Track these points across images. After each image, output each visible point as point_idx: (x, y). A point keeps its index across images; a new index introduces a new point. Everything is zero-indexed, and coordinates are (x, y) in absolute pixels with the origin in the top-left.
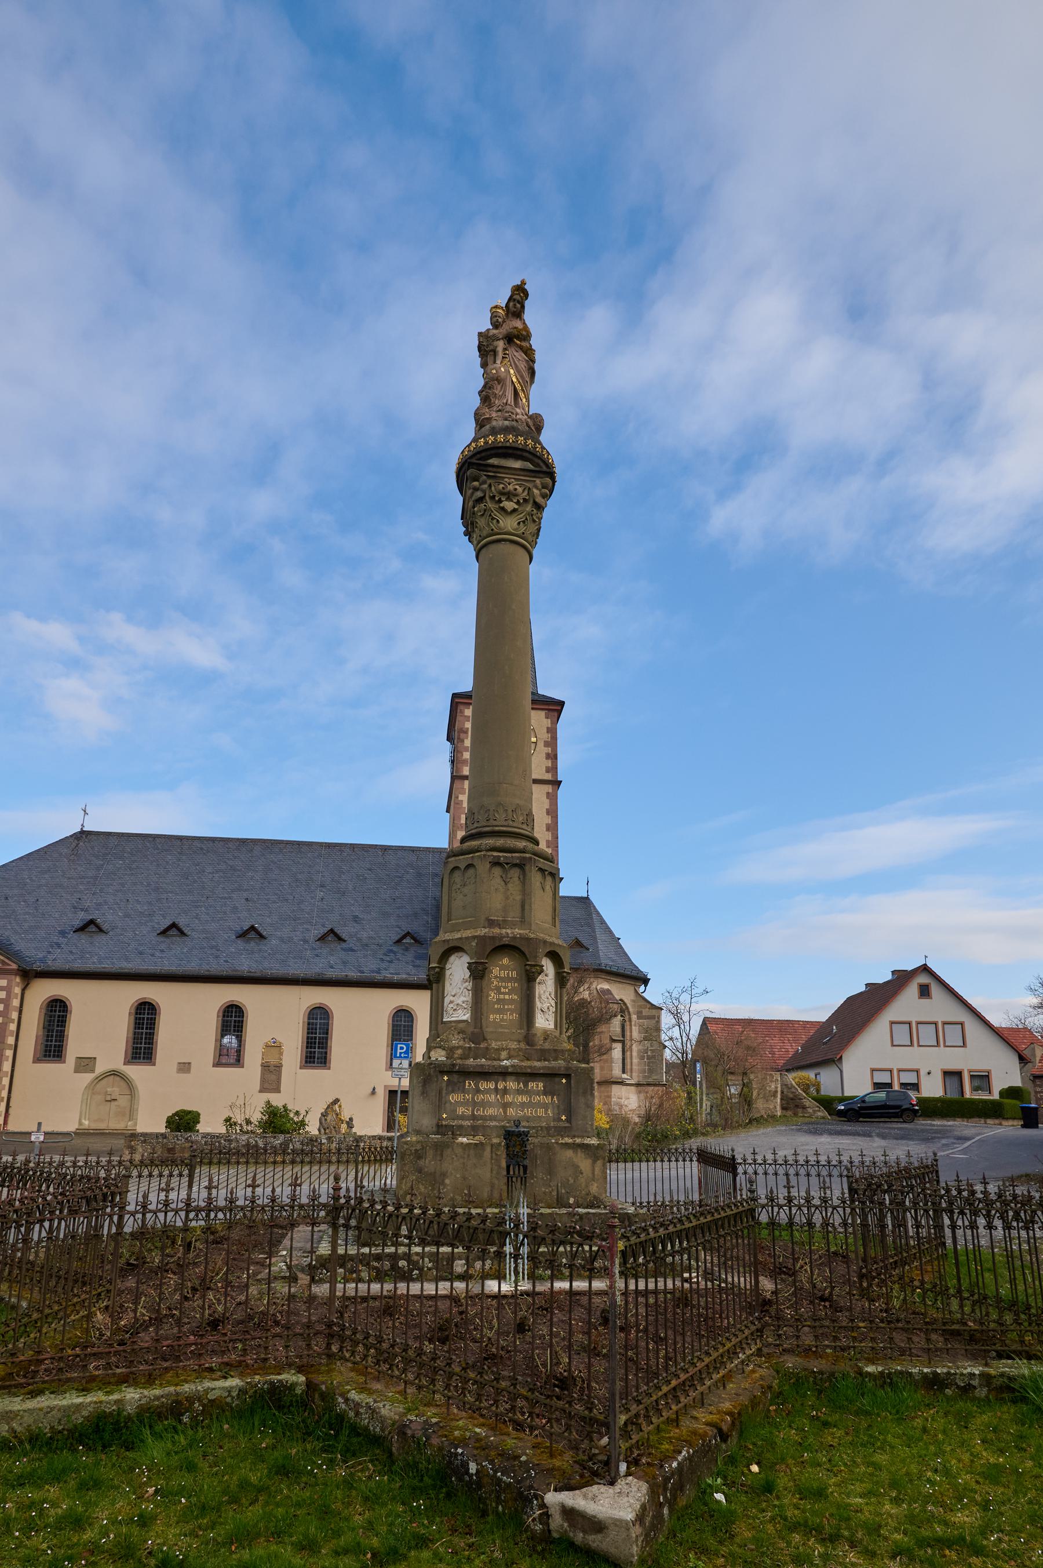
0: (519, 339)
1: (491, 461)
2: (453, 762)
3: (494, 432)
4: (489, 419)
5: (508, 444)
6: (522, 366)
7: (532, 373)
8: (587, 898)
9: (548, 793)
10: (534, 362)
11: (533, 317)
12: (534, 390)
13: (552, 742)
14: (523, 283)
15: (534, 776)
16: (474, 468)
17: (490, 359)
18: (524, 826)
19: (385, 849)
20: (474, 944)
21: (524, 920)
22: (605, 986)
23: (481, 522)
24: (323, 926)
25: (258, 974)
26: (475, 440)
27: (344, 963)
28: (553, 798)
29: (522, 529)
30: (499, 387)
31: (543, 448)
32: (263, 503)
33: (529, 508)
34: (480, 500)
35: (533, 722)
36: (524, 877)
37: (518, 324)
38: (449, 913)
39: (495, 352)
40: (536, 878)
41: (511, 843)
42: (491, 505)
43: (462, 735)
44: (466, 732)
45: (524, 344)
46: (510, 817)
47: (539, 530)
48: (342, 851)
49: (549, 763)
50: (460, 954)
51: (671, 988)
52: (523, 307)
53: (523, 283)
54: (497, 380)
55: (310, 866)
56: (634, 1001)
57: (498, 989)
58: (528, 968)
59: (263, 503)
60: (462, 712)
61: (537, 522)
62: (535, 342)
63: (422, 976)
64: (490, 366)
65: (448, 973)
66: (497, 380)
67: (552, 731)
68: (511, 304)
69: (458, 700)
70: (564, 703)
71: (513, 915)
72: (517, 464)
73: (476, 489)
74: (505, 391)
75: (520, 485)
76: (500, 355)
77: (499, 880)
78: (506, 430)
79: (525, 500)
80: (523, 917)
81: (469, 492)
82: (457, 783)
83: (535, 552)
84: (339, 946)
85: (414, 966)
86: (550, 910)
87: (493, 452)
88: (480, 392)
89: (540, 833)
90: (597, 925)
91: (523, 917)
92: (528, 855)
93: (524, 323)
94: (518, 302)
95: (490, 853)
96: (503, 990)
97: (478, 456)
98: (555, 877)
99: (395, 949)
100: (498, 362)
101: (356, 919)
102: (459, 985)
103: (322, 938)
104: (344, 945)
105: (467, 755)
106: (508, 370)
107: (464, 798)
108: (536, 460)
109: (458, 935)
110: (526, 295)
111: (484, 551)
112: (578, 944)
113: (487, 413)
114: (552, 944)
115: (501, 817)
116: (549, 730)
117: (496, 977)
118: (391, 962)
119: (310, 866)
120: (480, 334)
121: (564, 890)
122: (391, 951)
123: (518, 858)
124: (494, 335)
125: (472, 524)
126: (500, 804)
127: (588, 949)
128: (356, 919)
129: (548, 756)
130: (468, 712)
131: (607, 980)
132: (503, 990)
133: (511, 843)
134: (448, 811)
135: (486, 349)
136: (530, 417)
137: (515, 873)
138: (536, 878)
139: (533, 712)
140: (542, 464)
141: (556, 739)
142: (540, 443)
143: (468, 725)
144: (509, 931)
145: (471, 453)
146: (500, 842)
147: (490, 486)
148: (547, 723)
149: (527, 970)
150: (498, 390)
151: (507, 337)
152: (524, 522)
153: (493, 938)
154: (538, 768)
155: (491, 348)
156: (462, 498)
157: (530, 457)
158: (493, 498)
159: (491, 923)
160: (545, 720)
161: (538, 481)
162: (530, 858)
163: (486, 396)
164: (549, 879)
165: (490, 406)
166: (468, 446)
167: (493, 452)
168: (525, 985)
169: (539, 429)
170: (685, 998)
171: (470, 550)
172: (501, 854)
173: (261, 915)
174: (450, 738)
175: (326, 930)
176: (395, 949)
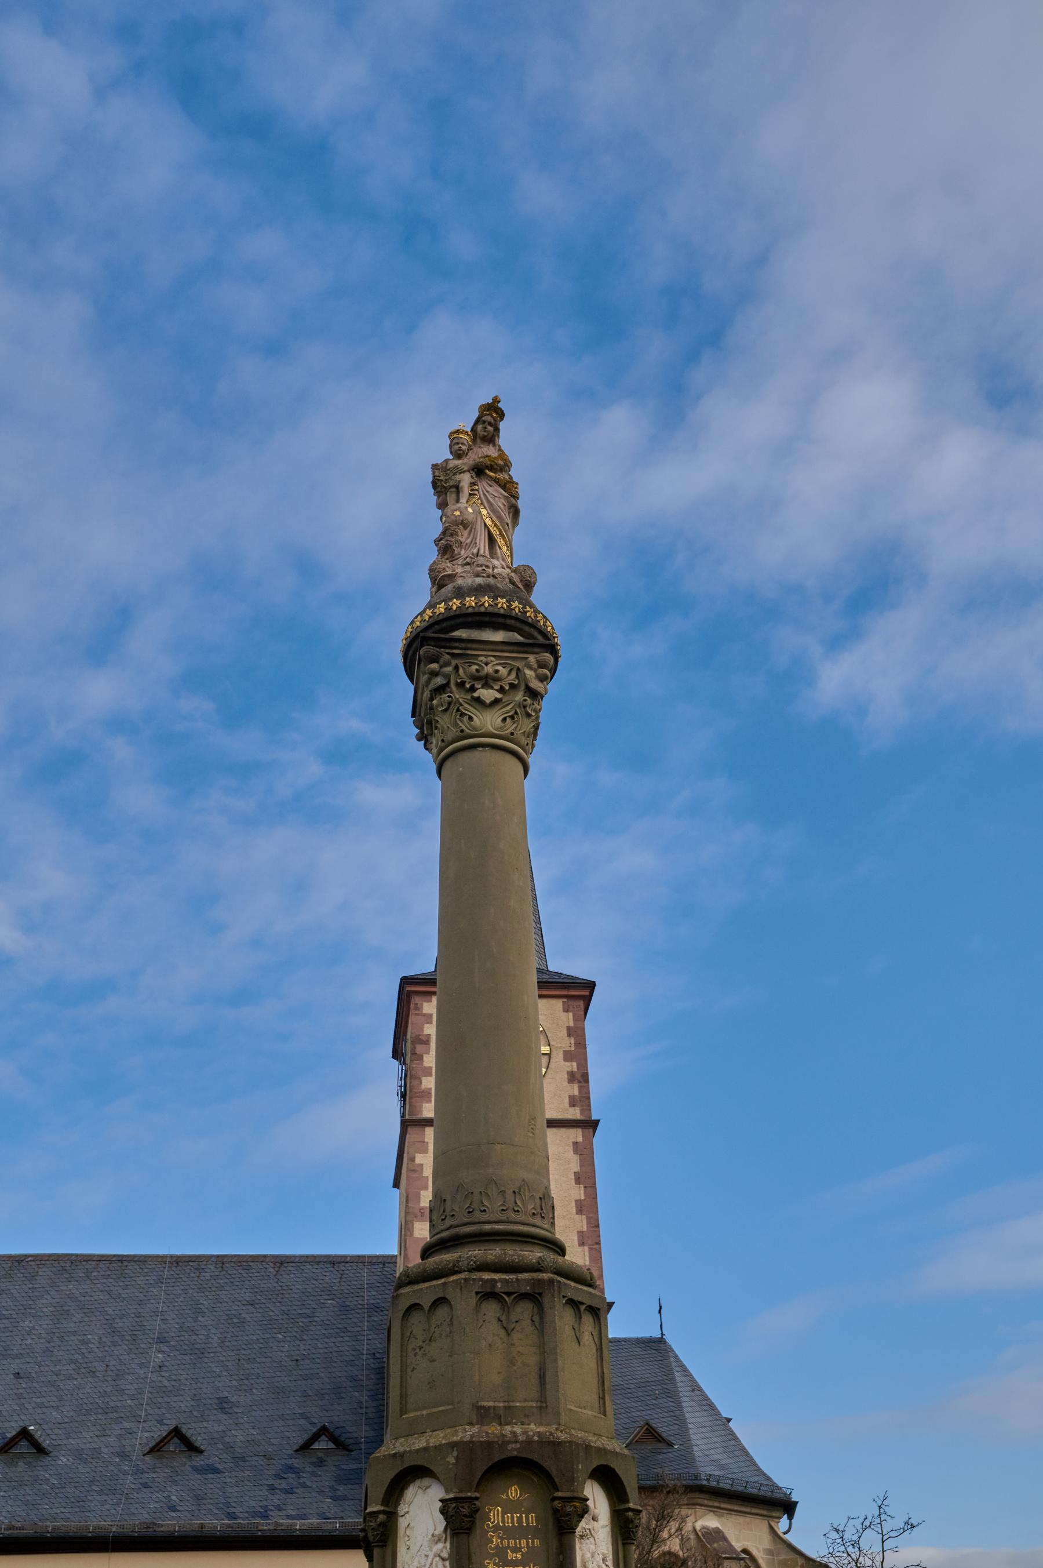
0: (492, 470)
1: (457, 634)
2: (403, 1095)
4: (452, 577)
5: (482, 609)
6: (500, 504)
7: (515, 512)
8: (661, 1341)
9: (576, 1144)
10: (516, 497)
11: (511, 437)
12: (518, 536)
13: (578, 1053)
14: (496, 400)
15: (551, 1114)
16: (430, 646)
17: (451, 498)
18: (537, 1221)
19: (281, 1262)
20: (451, 1460)
21: (545, 1404)
22: (710, 1522)
23: (444, 721)
24: (160, 1422)
25: (28, 1532)
26: (431, 605)
27: (198, 1498)
28: (584, 1152)
29: (510, 726)
31: (537, 612)
32: (100, 692)
33: (519, 696)
35: (542, 1019)
36: (541, 1318)
37: (492, 451)
38: (403, 1398)
39: (457, 489)
40: (563, 1319)
41: (513, 1253)
42: (458, 695)
43: (419, 1048)
44: (426, 1042)
45: (500, 476)
46: (511, 1205)
47: (536, 728)
48: (199, 1270)
49: (575, 1090)
50: (426, 1481)
51: (840, 1521)
52: (497, 430)
53: (496, 400)
54: (462, 523)
55: (140, 1303)
56: (769, 1552)
57: (501, 1552)
58: (557, 1504)
59: (100, 692)
60: (418, 1008)
61: (532, 716)
62: (515, 473)
63: (351, 1520)
64: (451, 506)
65: (402, 1523)
66: (462, 523)
67: (577, 1033)
68: (480, 427)
69: (412, 989)
70: (591, 986)
71: (525, 1396)
72: (499, 636)
73: (434, 674)
75: (504, 665)
76: (466, 491)
77: (494, 1327)
78: (478, 591)
80: (543, 1399)
81: (424, 679)
82: (412, 1135)
83: (531, 760)
84: (185, 1463)
85: (335, 1499)
86: (593, 1380)
87: (459, 621)
88: (437, 541)
89: (567, 1228)
90: (684, 1391)
91: (543, 1399)
92: (546, 1276)
93: (500, 450)
94: (490, 424)
95: (475, 1275)
96: (511, 1556)
97: (437, 627)
98: (598, 1311)
99: (296, 1462)
100: (463, 500)
101: (223, 1405)
102: (425, 1550)
103: (157, 1449)
104: (199, 1461)
105: (429, 1083)
106: (479, 507)
107: (426, 1161)
108: (527, 629)
109: (420, 1443)
110: (501, 415)
111: (448, 764)
112: (651, 1434)
114: (602, 1451)
115: (494, 1207)
116: (570, 1032)
117: (496, 1528)
118: (289, 1491)
119: (140, 1303)
120: (435, 467)
121: (617, 1327)
122: (290, 1468)
123: (528, 1281)
124: (456, 467)
125: (430, 723)
126: (491, 1181)
127: (670, 1445)
128: (223, 1405)
129: (572, 1077)
130: (430, 1007)
131: (715, 1510)
132: (511, 1556)
133: (513, 1253)
134: (396, 1185)
135: (444, 485)
136: (515, 571)
137: (524, 1311)
138: (563, 1319)
139: (542, 1004)
140: (536, 634)
143: (430, 1030)
144: (518, 1429)
145: (425, 624)
146: (494, 1252)
147: (456, 668)
148: (568, 1019)
149: (556, 1511)
150: (464, 536)
151: (477, 461)
152: (512, 717)
153: (488, 1445)
154: (556, 1101)
156: (412, 687)
157: (518, 625)
159: (483, 1415)
160: (564, 1016)
161: (532, 659)
162: (551, 1281)
164: (588, 1320)
165: (453, 558)
166: (421, 614)
167: (459, 621)
168: (554, 1544)
169: (529, 586)
170: (870, 1540)
171: (428, 759)
172: (496, 1276)
173: (41, 1406)
175: (164, 1431)
176: (296, 1462)
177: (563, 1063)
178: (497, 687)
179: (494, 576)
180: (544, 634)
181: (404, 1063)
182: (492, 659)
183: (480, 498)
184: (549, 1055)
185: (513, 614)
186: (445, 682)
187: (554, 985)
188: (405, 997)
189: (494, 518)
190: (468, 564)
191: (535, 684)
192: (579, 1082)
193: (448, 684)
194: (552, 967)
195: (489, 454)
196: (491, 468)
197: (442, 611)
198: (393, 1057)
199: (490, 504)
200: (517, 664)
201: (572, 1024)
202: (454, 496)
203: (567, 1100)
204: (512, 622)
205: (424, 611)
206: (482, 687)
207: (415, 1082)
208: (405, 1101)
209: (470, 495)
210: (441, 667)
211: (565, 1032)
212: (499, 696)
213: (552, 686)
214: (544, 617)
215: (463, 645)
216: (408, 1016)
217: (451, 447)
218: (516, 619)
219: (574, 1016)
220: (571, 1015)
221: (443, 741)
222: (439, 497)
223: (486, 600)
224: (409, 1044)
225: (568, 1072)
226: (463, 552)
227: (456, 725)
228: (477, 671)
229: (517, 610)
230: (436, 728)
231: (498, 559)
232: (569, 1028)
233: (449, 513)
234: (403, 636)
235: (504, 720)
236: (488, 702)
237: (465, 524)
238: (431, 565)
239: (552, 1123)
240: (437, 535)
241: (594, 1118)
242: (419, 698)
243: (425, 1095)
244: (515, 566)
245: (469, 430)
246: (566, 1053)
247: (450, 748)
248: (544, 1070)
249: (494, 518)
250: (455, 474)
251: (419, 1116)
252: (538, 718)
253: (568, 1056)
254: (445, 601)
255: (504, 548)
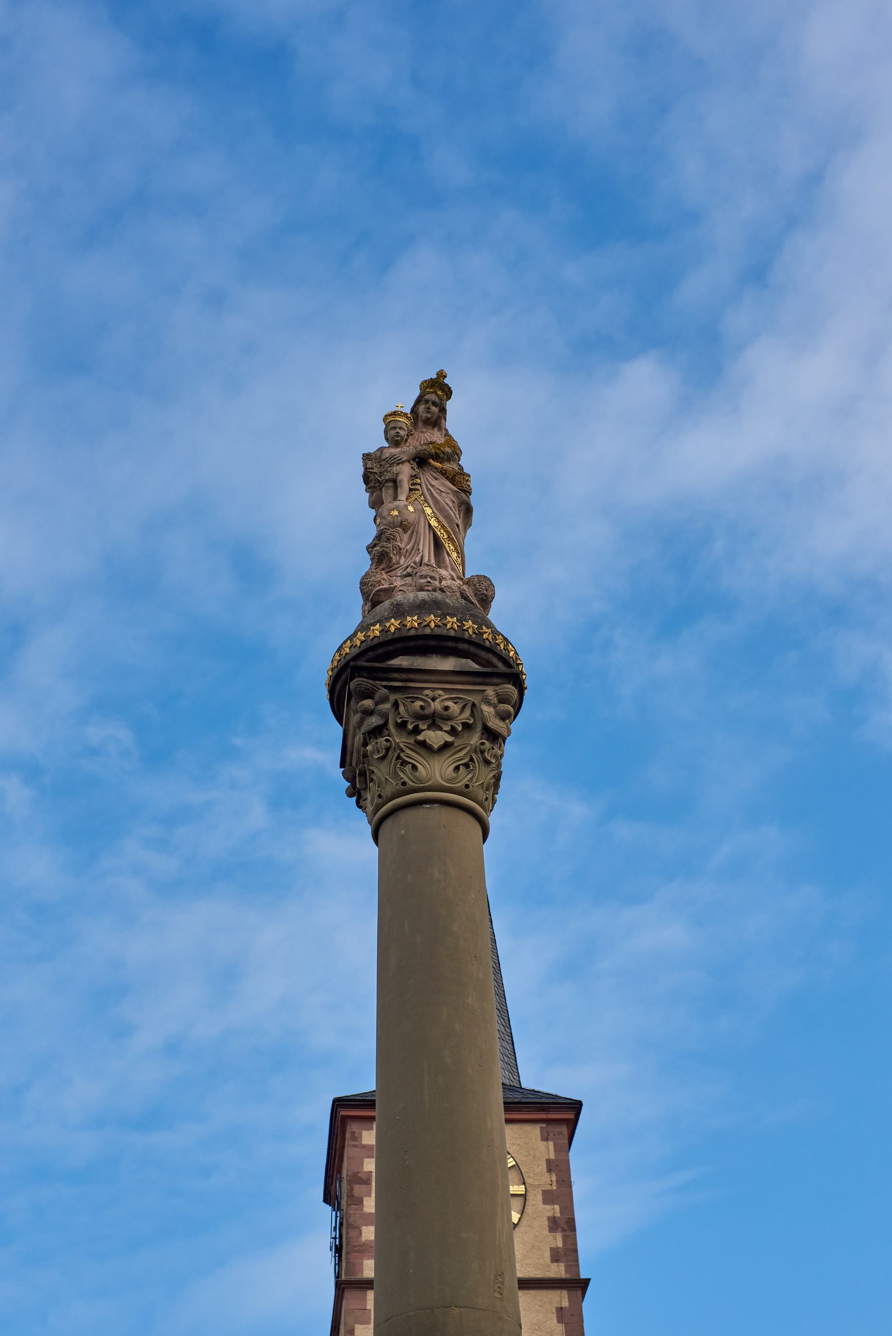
0: (440, 460)
2: (338, 1250)
3: (399, 611)
4: (389, 591)
5: (427, 631)
6: (448, 501)
7: (468, 511)
9: (560, 1310)
10: (468, 492)
12: (472, 540)
13: (561, 1193)
14: (442, 375)
15: (522, 1272)
16: (363, 678)
17: (387, 494)
23: (381, 771)
26: (363, 627)
29: (464, 777)
30: (406, 537)
31: (495, 633)
33: (475, 739)
34: (377, 731)
37: (436, 437)
42: (399, 739)
43: (358, 1189)
45: (447, 466)
47: (497, 778)
52: (443, 410)
53: (442, 375)
60: (356, 1138)
62: (466, 462)
67: (559, 1168)
68: (422, 408)
69: (347, 1112)
70: (576, 1107)
72: (448, 664)
73: (368, 713)
74: (417, 543)
75: (456, 700)
76: (406, 486)
78: (422, 608)
79: (467, 726)
81: (355, 718)
82: (350, 1300)
83: (494, 820)
88: (370, 548)
93: (447, 434)
94: (434, 404)
100: (402, 497)
105: (369, 1233)
106: (421, 506)
108: (484, 654)
110: (448, 393)
113: (384, 580)
116: (551, 1166)
120: (367, 457)
124: (392, 456)
125: (363, 774)
130: (369, 1137)
135: (377, 478)
136: (468, 583)
139: (512, 1133)
140: (495, 660)
141: (569, 1185)
142: (489, 625)
143: (370, 1165)
145: (356, 651)
147: (396, 705)
148: (547, 1150)
150: (403, 541)
151: (418, 453)
152: (467, 765)
154: (530, 1253)
155: (388, 476)
156: (339, 730)
157: (473, 649)
158: (402, 726)
160: (542, 1145)
161: (490, 691)
163: (381, 554)
166: (350, 638)
169: (486, 601)
174: (330, 1197)
177: (541, 1206)
178: (447, 728)
179: (441, 590)
180: (506, 661)
181: (339, 1209)
182: (440, 692)
183: (423, 494)
184: (524, 1196)
185: (466, 635)
186: (381, 722)
187: (527, 1106)
188: (338, 1123)
189: (441, 518)
190: (409, 575)
191: (495, 724)
192: (564, 1230)
193: (385, 725)
194: (528, 1082)
195: (434, 439)
196: (436, 457)
197: (377, 633)
198: (326, 1200)
199: (436, 501)
200: (470, 698)
201: (552, 1156)
202: (391, 491)
203: (547, 1254)
204: (465, 646)
205: (355, 633)
206: (429, 728)
207: (353, 1233)
208: (340, 1257)
209: (411, 490)
210: (377, 704)
211: (543, 1167)
212: (450, 739)
213: (516, 726)
214: (505, 639)
215: (404, 676)
216: (343, 1147)
217: (386, 432)
218: (469, 642)
219: (555, 1145)
220: (551, 1144)
221: (380, 796)
222: (372, 494)
223: (432, 619)
224: (345, 1184)
225: (549, 1218)
226: (402, 561)
227: (396, 775)
228: (422, 707)
229: (470, 631)
230: (372, 780)
231: (446, 568)
232: (549, 1161)
233: (385, 513)
234: (329, 665)
235: (457, 768)
236: (436, 747)
237: (404, 526)
238: (363, 578)
239: (526, 1284)
240: (370, 538)
241: (583, 1276)
242: (349, 743)
243: (364, 1249)
244: (468, 576)
245: (408, 411)
246: (545, 1193)
247: (389, 805)
248: (515, 1217)
249: (441, 518)
250: (392, 465)
251: (359, 1277)
252: (499, 765)
253: (549, 1197)
254: (380, 621)
255: (454, 555)
